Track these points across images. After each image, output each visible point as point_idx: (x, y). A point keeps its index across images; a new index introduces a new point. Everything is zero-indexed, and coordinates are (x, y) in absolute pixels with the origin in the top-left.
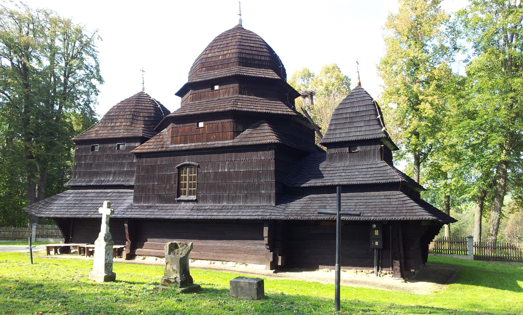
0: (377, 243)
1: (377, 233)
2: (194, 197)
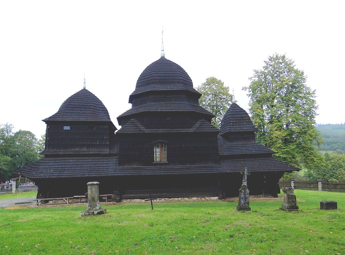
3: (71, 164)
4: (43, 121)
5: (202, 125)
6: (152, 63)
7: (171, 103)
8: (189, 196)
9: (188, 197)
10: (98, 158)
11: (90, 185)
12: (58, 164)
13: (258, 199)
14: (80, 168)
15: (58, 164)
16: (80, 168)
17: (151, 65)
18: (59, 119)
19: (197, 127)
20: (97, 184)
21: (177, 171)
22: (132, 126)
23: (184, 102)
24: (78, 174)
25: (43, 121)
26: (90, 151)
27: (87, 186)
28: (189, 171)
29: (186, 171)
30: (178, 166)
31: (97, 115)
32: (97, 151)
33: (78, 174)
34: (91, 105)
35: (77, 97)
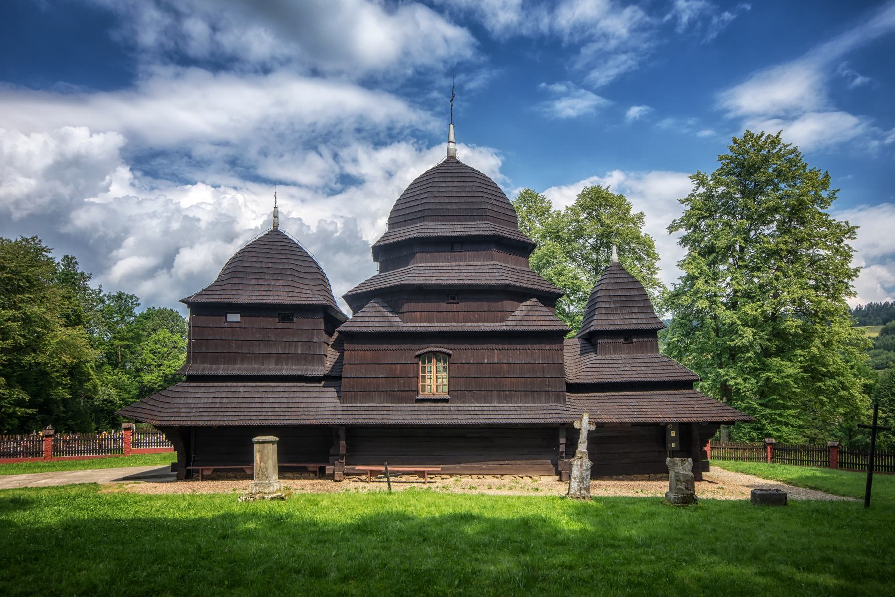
0: (673, 445)
1: (673, 434)
2: (443, 392)
3: (241, 395)
4: (183, 301)
5: (530, 314)
6: (426, 172)
7: (462, 264)
8: (496, 472)
9: (494, 475)
10: (299, 384)
11: (258, 443)
12: (212, 395)
13: (137, 485)
14: (259, 405)
15: (212, 395)
16: (259, 405)
17: (422, 176)
18: (216, 299)
19: (518, 318)
20: (273, 442)
21: (470, 417)
22: (374, 314)
23: (492, 263)
24: (254, 418)
25: (183, 301)
26: (282, 369)
27: (252, 444)
28: (495, 417)
29: (489, 417)
30: (473, 406)
31: (300, 290)
32: (298, 370)
33: (254, 418)
34: (287, 266)
35: (258, 250)
